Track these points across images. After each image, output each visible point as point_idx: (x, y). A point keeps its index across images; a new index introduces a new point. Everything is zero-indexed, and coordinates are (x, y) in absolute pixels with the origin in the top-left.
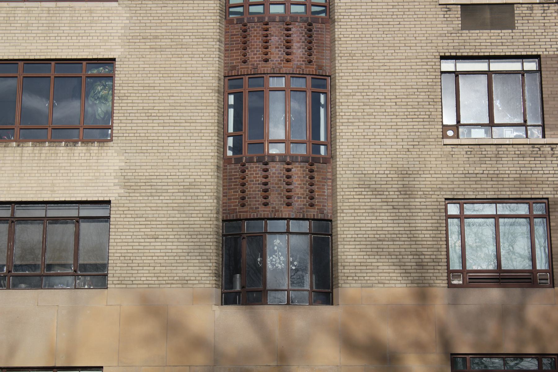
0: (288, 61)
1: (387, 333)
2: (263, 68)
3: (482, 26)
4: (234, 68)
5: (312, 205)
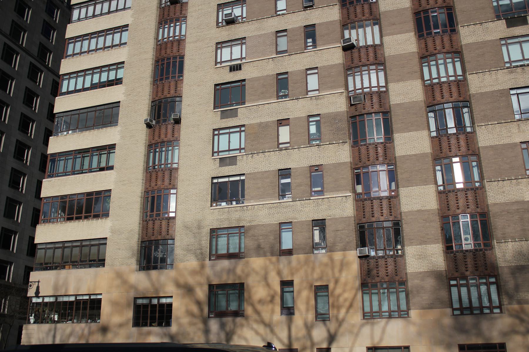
0: (459, 150)
1: (191, 281)
2: (368, 163)
3: (226, 165)
4: (147, 189)
5: (168, 234)
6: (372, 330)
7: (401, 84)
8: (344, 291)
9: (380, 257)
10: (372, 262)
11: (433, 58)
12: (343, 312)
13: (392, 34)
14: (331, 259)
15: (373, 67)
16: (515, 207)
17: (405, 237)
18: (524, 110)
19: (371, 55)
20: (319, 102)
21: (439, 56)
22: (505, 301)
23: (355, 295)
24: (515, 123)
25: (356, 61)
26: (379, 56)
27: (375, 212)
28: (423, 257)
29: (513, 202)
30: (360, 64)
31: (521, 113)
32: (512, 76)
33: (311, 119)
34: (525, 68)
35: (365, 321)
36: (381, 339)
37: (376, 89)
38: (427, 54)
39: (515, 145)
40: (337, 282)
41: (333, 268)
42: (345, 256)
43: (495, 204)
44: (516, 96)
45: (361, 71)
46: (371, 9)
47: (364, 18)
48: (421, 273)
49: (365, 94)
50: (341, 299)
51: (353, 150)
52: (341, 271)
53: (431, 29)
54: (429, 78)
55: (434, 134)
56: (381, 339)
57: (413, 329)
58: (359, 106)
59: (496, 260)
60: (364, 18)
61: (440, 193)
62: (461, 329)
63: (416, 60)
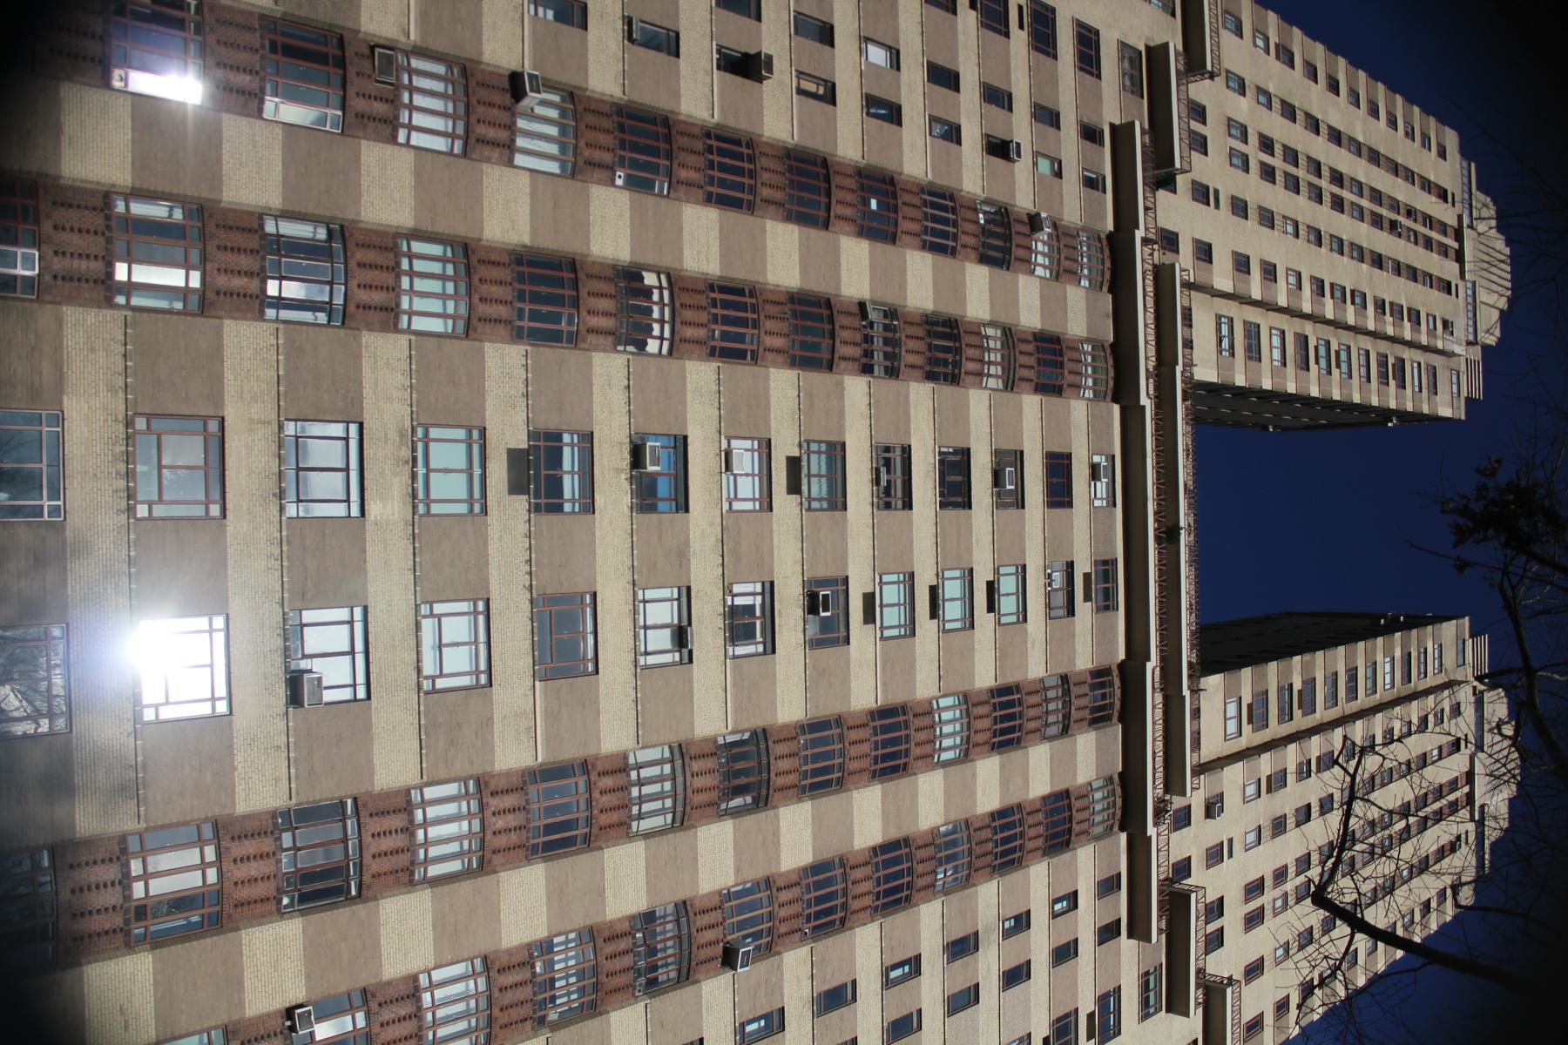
7: (408, 180)
11: (463, 291)
13: (533, 195)
18: (305, 445)
19: (492, 133)
21: (482, 981)
24: (274, 416)
25: (483, 94)
26: (487, 151)
29: (61, 368)
30: (473, 101)
31: (297, 437)
32: (393, 435)
34: (408, 468)
37: (405, 305)
38: (474, 259)
39: (220, 403)
43: (60, 323)
44: (341, 434)
45: (455, 117)
46: (601, 166)
47: (582, 145)
49: (397, 87)
51: (251, 13)
53: (531, 302)
54: (414, 122)
55: (270, 227)
58: (367, 63)
60: (582, 145)
63: (462, 230)
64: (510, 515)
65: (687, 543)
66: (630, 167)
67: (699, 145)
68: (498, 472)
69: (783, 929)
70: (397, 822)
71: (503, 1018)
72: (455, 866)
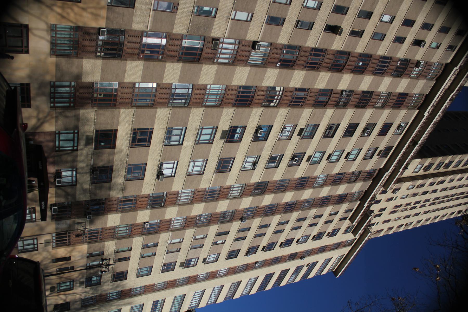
6: (43, 30)
8: (75, 14)
9: (97, 42)
10: (95, 37)
12: (59, 10)
14: (102, 8)
15: (236, 48)
16: (115, 121)
17: (108, 61)
20: (225, 18)
22: (59, 111)
23: (71, 22)
27: (131, 44)
28: (93, 69)
33: (214, 9)
34: (196, 136)
35: (50, 25)
36: (35, 35)
40: (84, 9)
41: (94, 8)
42: (103, 18)
43: (119, 112)
44: (61, 142)
48: (82, 67)
50: (69, 11)
52: (92, 14)
56: (35, 35)
57: (43, 57)
59: (84, 109)
61: (134, 84)
62: (42, 85)
64: (219, 143)
65: (264, 147)
66: (287, 48)
67: (308, 54)
68: (219, 135)
69: (324, 65)
70: (202, 92)
71: (239, 58)
72: (227, 61)
